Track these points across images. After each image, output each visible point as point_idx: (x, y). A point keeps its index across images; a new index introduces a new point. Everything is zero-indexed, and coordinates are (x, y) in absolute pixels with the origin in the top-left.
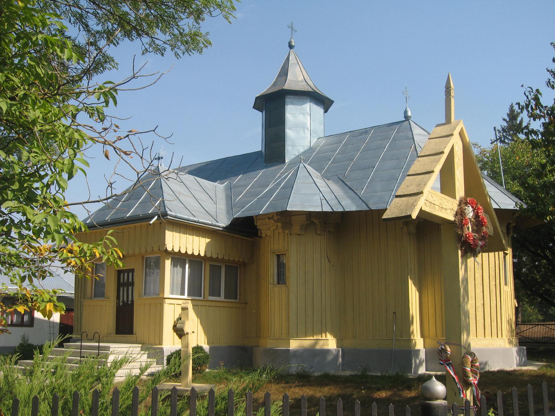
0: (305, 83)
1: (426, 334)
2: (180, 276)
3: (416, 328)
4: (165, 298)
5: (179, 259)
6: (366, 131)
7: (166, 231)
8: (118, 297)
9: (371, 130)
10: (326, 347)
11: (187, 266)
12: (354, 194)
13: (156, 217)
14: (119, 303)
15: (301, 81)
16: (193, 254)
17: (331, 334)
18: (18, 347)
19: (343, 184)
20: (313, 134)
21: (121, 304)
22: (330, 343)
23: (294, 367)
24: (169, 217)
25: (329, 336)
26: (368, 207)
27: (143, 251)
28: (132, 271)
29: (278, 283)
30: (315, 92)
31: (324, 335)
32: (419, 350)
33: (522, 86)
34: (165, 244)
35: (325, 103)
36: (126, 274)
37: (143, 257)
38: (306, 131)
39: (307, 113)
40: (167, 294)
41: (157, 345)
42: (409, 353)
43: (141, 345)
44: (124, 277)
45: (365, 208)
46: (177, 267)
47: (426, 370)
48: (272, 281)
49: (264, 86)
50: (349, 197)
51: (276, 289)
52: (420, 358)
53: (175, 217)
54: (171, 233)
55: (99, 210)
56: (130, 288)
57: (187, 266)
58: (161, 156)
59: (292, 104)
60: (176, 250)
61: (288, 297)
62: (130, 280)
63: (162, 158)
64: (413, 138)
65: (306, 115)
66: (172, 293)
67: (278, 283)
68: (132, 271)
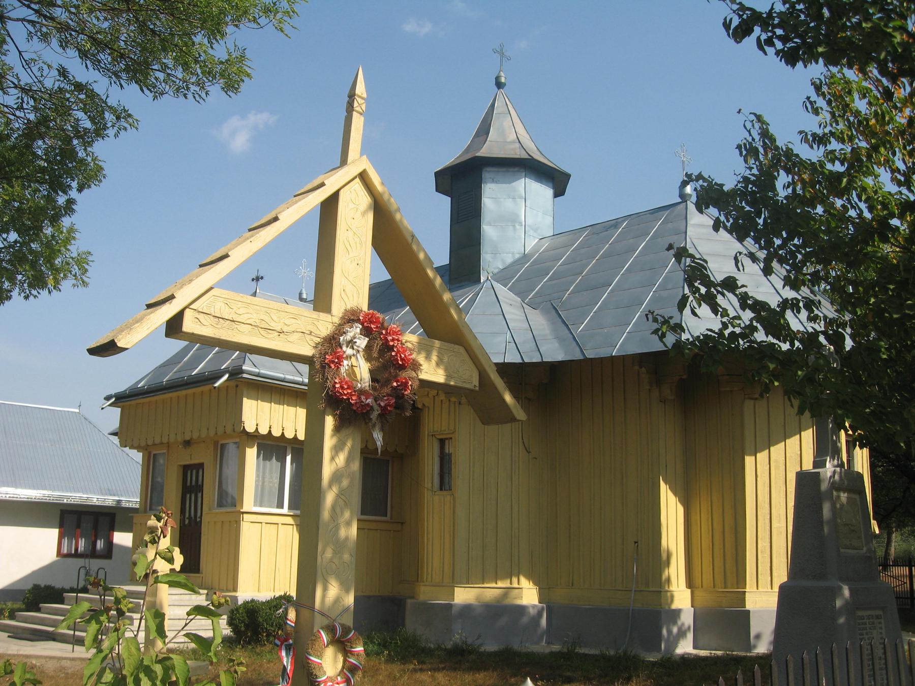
0: (518, 145)
1: (698, 582)
2: (277, 475)
3: (676, 572)
4: (243, 513)
5: (272, 446)
6: (615, 224)
7: (245, 400)
8: (183, 511)
9: (624, 221)
10: (518, 602)
11: (289, 458)
12: (567, 331)
13: (226, 376)
14: (184, 521)
15: (512, 142)
16: (295, 438)
17: (529, 577)
18: (29, 591)
19: (556, 315)
20: (530, 232)
21: (187, 522)
22: (528, 594)
23: (458, 635)
24: (245, 375)
25: (525, 583)
26: (583, 354)
27: (212, 433)
28: (201, 466)
29: (441, 489)
30: (533, 159)
31: (515, 580)
32: (678, 612)
33: (739, 112)
34: (241, 422)
35: (557, 180)
36: (194, 472)
37: (216, 443)
38: (518, 227)
39: (520, 197)
40: (248, 503)
41: (230, 591)
42: (658, 614)
43: (206, 591)
44: (192, 479)
45: (578, 356)
46: (270, 459)
47: (694, 648)
48: (430, 485)
49: (450, 155)
50: (557, 338)
51: (436, 498)
52: (679, 623)
53: (258, 375)
54: (254, 402)
55: (160, 366)
56: (200, 495)
57: (289, 458)
58: (261, 274)
59: (493, 181)
60: (263, 431)
61: (454, 512)
62: (200, 483)
63: (262, 278)
64: (686, 232)
65: (518, 200)
66: (259, 501)
67: (441, 489)
68: (201, 466)
